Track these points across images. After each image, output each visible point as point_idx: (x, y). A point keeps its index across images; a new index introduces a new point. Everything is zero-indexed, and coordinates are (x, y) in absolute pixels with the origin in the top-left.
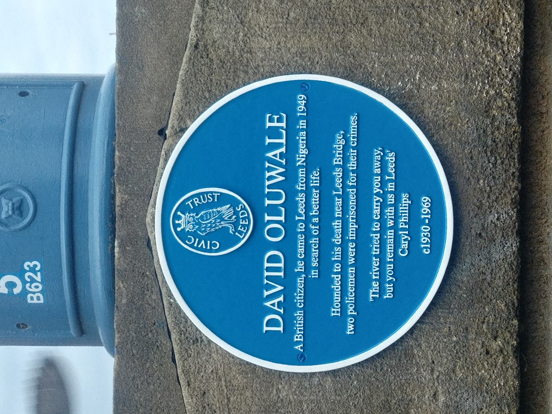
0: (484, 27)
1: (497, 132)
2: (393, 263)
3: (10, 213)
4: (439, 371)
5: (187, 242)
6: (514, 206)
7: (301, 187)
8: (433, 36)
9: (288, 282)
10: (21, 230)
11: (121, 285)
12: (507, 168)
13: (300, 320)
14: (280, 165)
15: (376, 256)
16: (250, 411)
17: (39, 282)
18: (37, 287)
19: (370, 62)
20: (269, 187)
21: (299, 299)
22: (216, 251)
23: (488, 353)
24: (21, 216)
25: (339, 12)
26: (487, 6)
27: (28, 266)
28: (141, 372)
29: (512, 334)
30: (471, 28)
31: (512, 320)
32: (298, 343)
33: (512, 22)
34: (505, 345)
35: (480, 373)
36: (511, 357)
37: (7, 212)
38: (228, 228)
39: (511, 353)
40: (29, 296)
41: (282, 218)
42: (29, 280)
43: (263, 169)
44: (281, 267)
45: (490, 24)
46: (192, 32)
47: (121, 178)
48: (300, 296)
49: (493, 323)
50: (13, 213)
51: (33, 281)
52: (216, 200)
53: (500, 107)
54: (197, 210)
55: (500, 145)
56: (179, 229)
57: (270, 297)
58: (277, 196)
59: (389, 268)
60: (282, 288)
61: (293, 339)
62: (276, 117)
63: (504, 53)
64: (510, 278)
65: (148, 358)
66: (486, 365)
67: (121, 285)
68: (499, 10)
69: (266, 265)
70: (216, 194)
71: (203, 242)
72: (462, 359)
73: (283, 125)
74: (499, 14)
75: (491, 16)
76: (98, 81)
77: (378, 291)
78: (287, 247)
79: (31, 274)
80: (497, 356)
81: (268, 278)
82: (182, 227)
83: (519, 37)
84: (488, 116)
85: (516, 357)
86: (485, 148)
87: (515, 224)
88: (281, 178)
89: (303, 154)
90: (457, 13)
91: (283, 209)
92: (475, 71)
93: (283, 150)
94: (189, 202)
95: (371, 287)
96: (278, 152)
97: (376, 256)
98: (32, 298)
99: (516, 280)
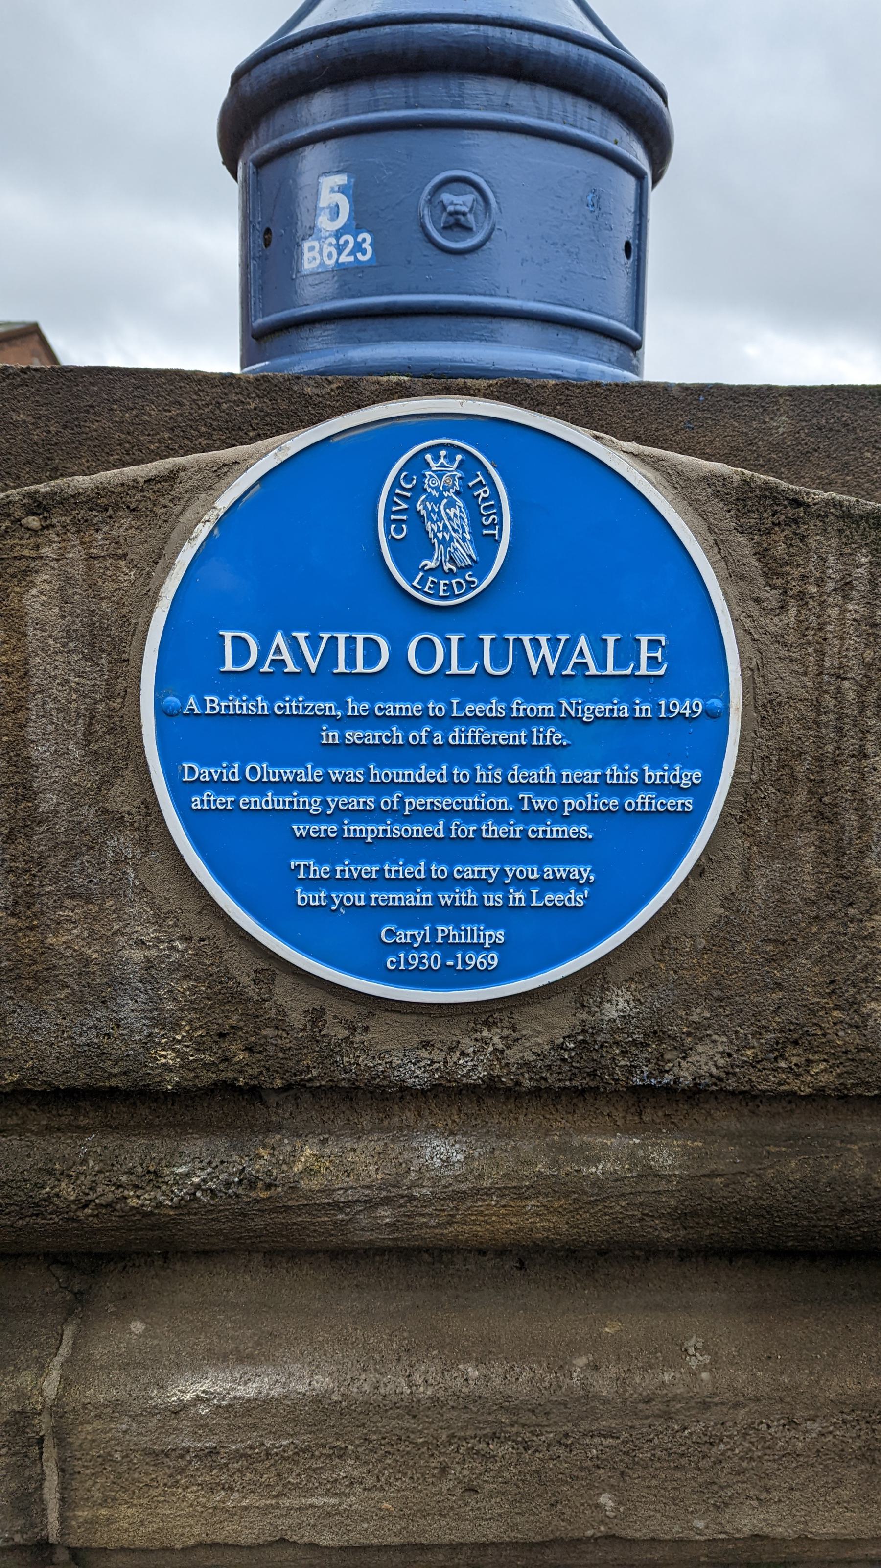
0: (806, 1029)
1: (617, 1051)
2: (368, 905)
3: (451, 208)
4: (186, 950)
5: (404, 474)
6: (487, 1080)
7: (518, 709)
8: (794, 940)
9: (326, 682)
10: (423, 227)
11: (334, 386)
12: (554, 1068)
13: (248, 708)
14: (562, 664)
15: (381, 872)
16: (102, 599)
17: (337, 260)
18: (330, 255)
19: (752, 828)
20: (518, 641)
21: (291, 707)
22: (387, 532)
23: (222, 1035)
24: (445, 228)
25: (846, 771)
26: (841, 1034)
27: (364, 240)
28: (191, 417)
29: (256, 1077)
30: (805, 1006)
31: (282, 1078)
32: (202, 704)
33: (812, 1076)
34: (236, 1067)
35: (184, 1023)
36: (214, 1076)
37: (452, 204)
38: (430, 558)
39: (223, 1076)
40: (316, 244)
41: (454, 669)
42: (341, 242)
43: (553, 629)
44: (356, 668)
45: (809, 1038)
46: (820, 495)
47: (511, 388)
48: (297, 707)
49: (276, 1045)
50: (451, 214)
51: (340, 249)
52: (485, 532)
53: (662, 1056)
54: (466, 493)
55: (596, 1056)
56: (428, 457)
57: (294, 645)
58: (498, 659)
59: (358, 898)
60: (313, 671)
61: (210, 693)
62: (659, 654)
63: (758, 1062)
64: (357, 1075)
65: (214, 430)
66: (200, 1033)
67: (334, 386)
68: (833, 1054)
69: (360, 637)
70: (496, 532)
71: (404, 506)
72: (209, 991)
73: (643, 671)
74: (826, 1053)
75: (824, 1040)
76: (636, 369)
77: (312, 876)
78: (397, 679)
79: (351, 245)
80: (216, 1053)
81: (333, 640)
82: (432, 463)
83: (782, 1088)
84: (646, 1035)
85: (215, 1084)
86: (590, 1031)
87: (455, 1081)
88: (535, 667)
89: (583, 712)
90: (832, 982)
91: (473, 671)
92: (727, 1013)
93: (593, 670)
94: (481, 478)
95: (320, 862)
96: (589, 659)
97: (381, 872)
98: (312, 249)
99: (354, 1084)
